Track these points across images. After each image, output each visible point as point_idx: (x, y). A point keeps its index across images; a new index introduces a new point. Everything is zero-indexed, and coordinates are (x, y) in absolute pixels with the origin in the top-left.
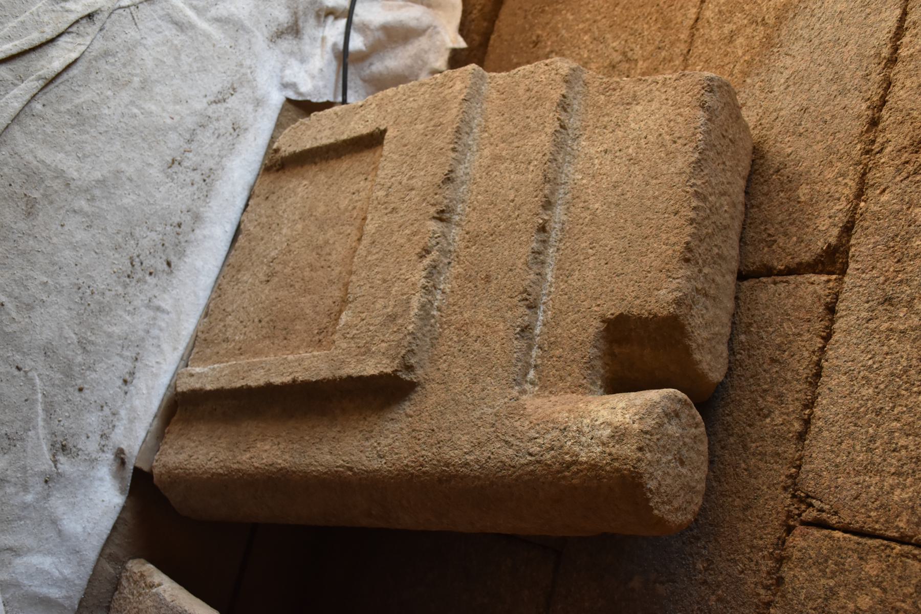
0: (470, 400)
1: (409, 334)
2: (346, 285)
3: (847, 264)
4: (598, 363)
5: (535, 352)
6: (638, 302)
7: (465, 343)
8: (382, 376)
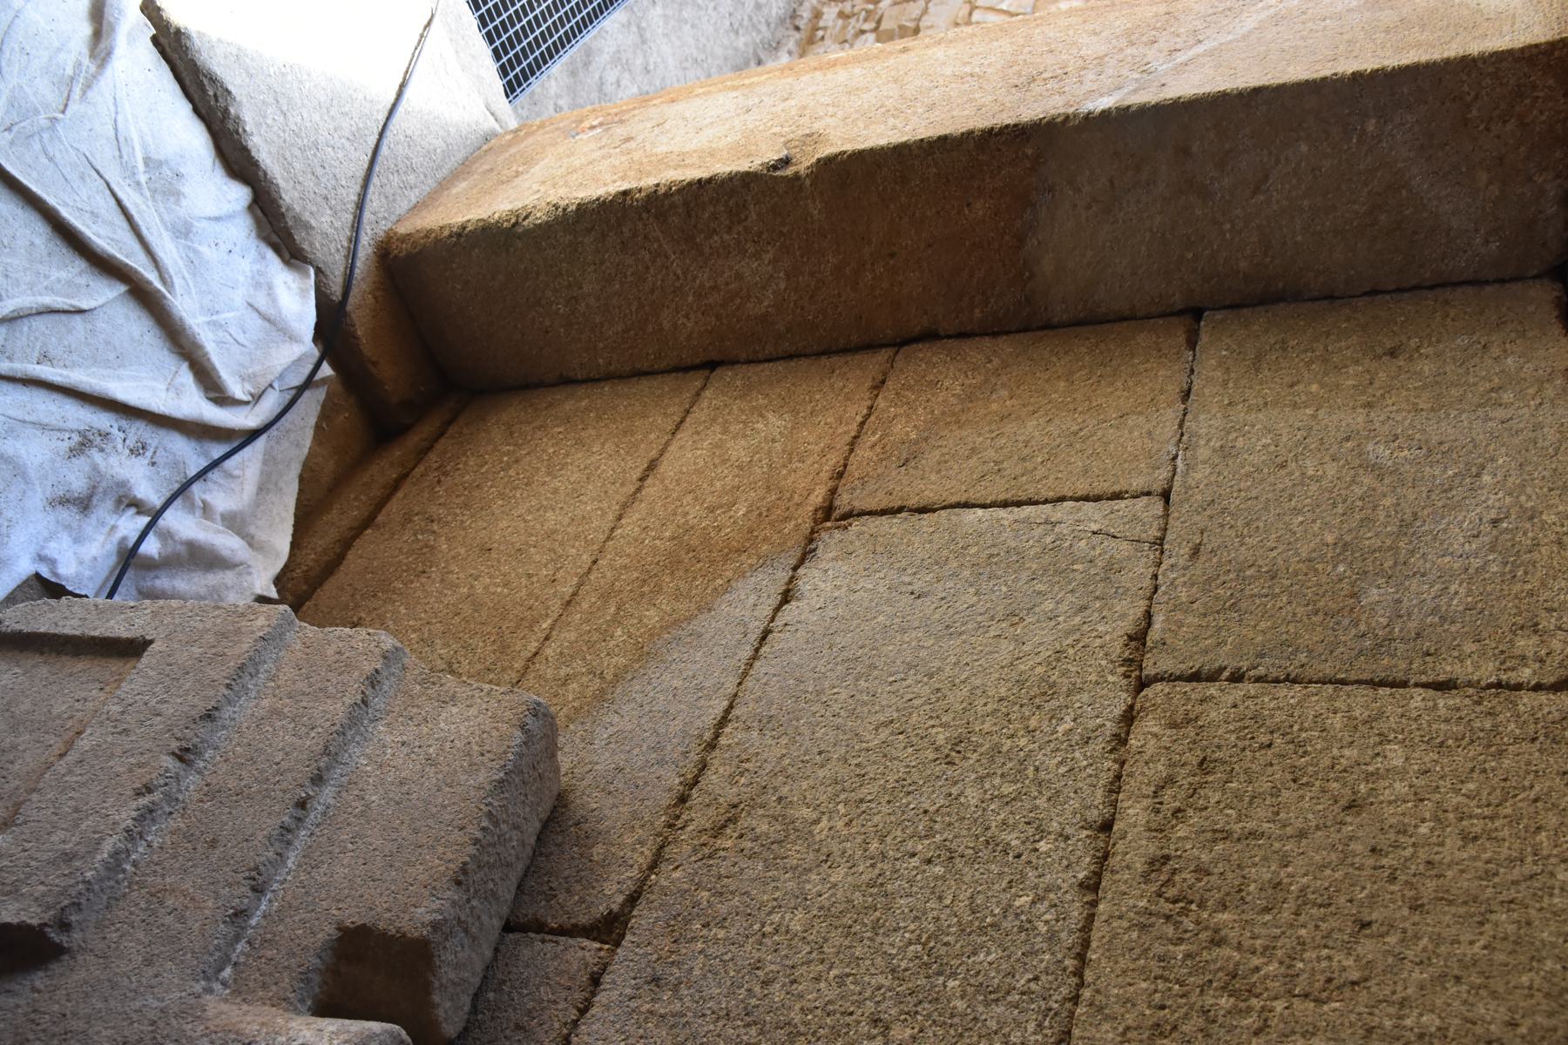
0: (134, 986)
1: (84, 882)
2: (18, 805)
3: (623, 936)
4: (317, 978)
5: (241, 946)
6: (388, 915)
7: (154, 913)
8: (23, 928)
